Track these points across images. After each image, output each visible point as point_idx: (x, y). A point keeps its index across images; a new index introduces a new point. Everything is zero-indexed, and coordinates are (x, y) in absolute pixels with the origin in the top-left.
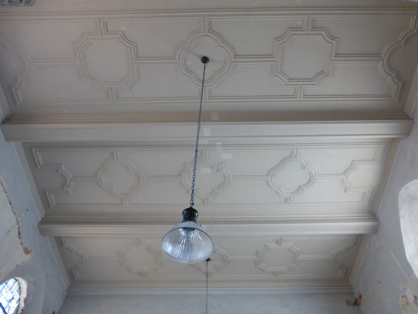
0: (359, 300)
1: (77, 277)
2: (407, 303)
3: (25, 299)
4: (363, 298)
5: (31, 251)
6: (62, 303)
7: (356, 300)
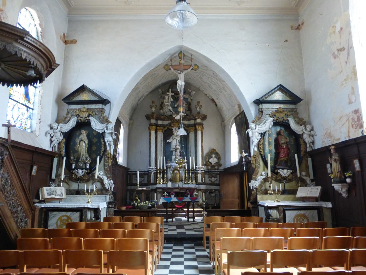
0: (301, 26)
1: (72, 5)
2: (334, 32)
3: (39, 24)
4: (305, 24)
5: (223, 88)
6: (67, 26)
7: (299, 25)
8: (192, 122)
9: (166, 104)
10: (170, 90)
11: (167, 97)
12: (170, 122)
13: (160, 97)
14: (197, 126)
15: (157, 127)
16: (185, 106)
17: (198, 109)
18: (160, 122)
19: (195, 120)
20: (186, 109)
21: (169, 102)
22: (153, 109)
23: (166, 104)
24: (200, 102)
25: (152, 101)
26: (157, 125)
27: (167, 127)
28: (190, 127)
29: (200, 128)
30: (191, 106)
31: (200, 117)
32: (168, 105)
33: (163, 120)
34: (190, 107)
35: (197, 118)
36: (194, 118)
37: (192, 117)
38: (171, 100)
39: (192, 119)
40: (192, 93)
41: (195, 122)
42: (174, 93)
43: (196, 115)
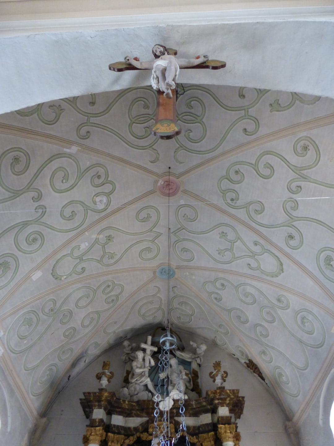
5: (279, 300)
8: (206, 419)
9: (138, 371)
10: (150, 338)
11: (140, 355)
12: (145, 419)
13: (126, 360)
14: (222, 428)
15: (107, 435)
16: (184, 377)
17: (218, 380)
18: (118, 420)
19: (214, 411)
20: (188, 385)
21: (145, 367)
22: (104, 382)
23: (138, 371)
24: (221, 363)
25: (104, 362)
26: (108, 428)
27: (135, 437)
28: (200, 435)
29: (231, 432)
30: (199, 380)
31: (225, 399)
32: (142, 375)
33: (127, 414)
34: (198, 382)
35: (219, 404)
36: (209, 407)
37: (204, 404)
38: (150, 363)
39: (206, 411)
40: (200, 348)
41: (212, 419)
42: (156, 346)
43: (215, 393)
